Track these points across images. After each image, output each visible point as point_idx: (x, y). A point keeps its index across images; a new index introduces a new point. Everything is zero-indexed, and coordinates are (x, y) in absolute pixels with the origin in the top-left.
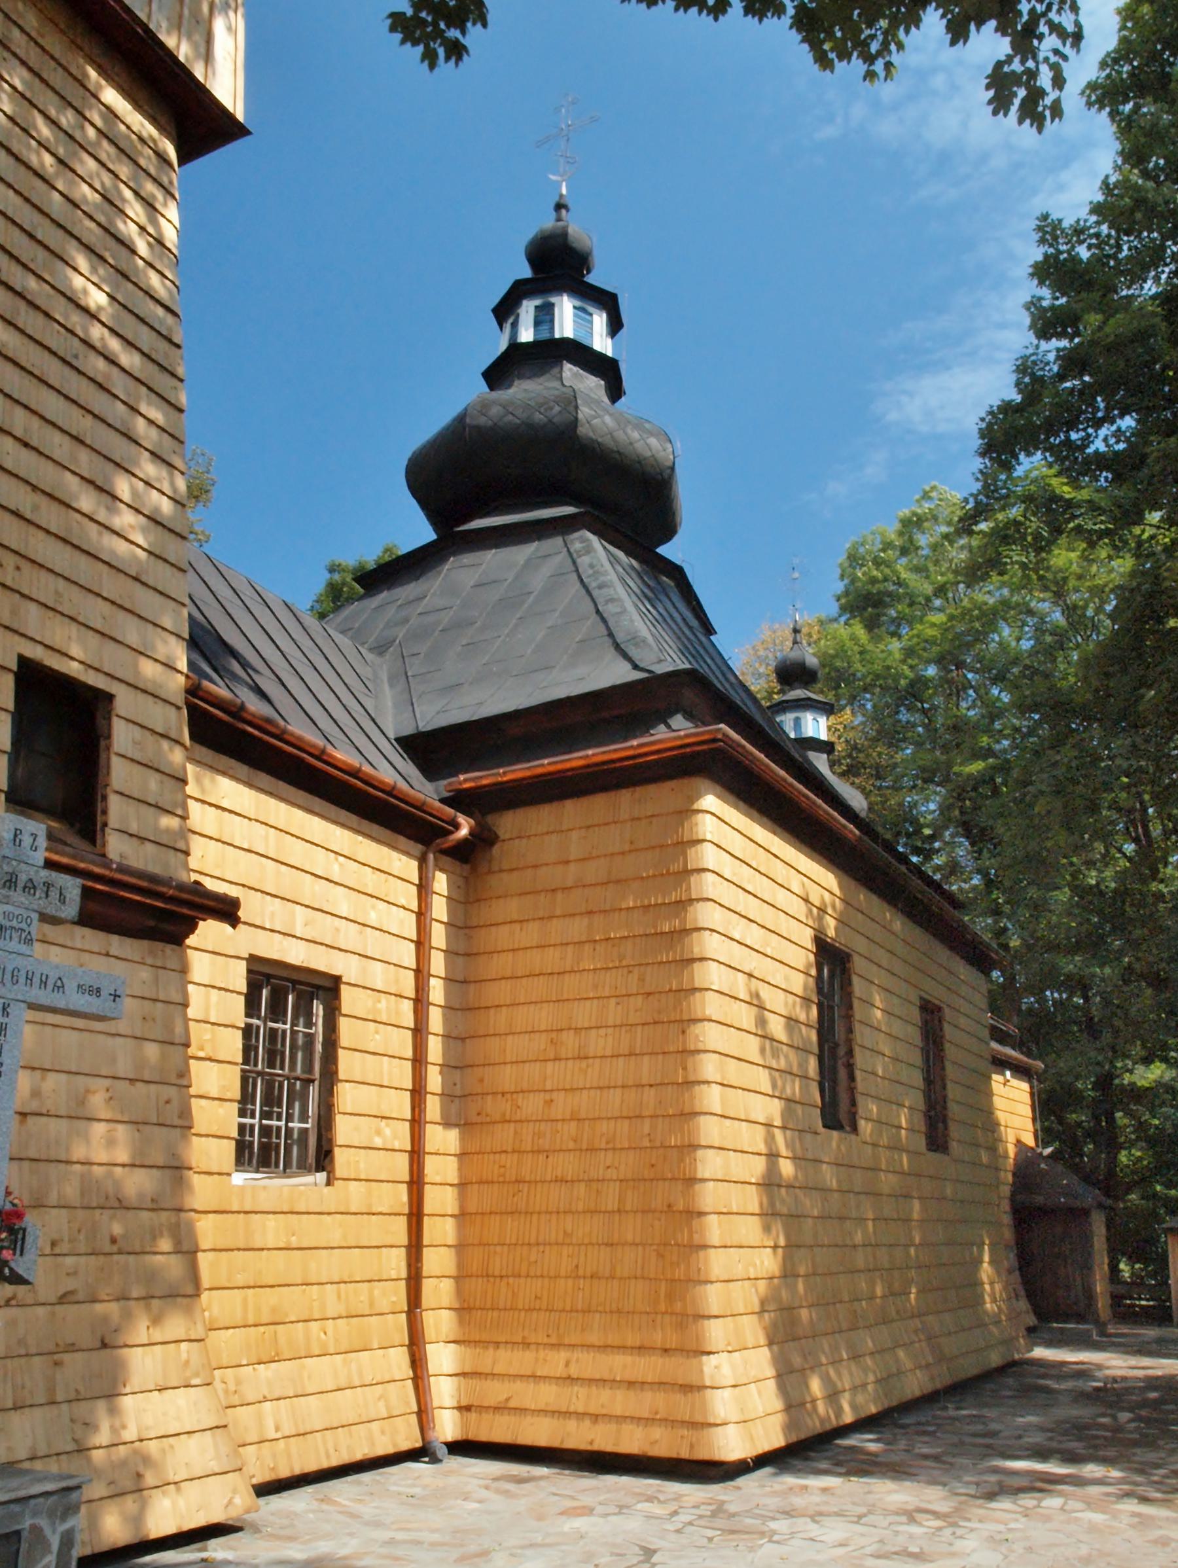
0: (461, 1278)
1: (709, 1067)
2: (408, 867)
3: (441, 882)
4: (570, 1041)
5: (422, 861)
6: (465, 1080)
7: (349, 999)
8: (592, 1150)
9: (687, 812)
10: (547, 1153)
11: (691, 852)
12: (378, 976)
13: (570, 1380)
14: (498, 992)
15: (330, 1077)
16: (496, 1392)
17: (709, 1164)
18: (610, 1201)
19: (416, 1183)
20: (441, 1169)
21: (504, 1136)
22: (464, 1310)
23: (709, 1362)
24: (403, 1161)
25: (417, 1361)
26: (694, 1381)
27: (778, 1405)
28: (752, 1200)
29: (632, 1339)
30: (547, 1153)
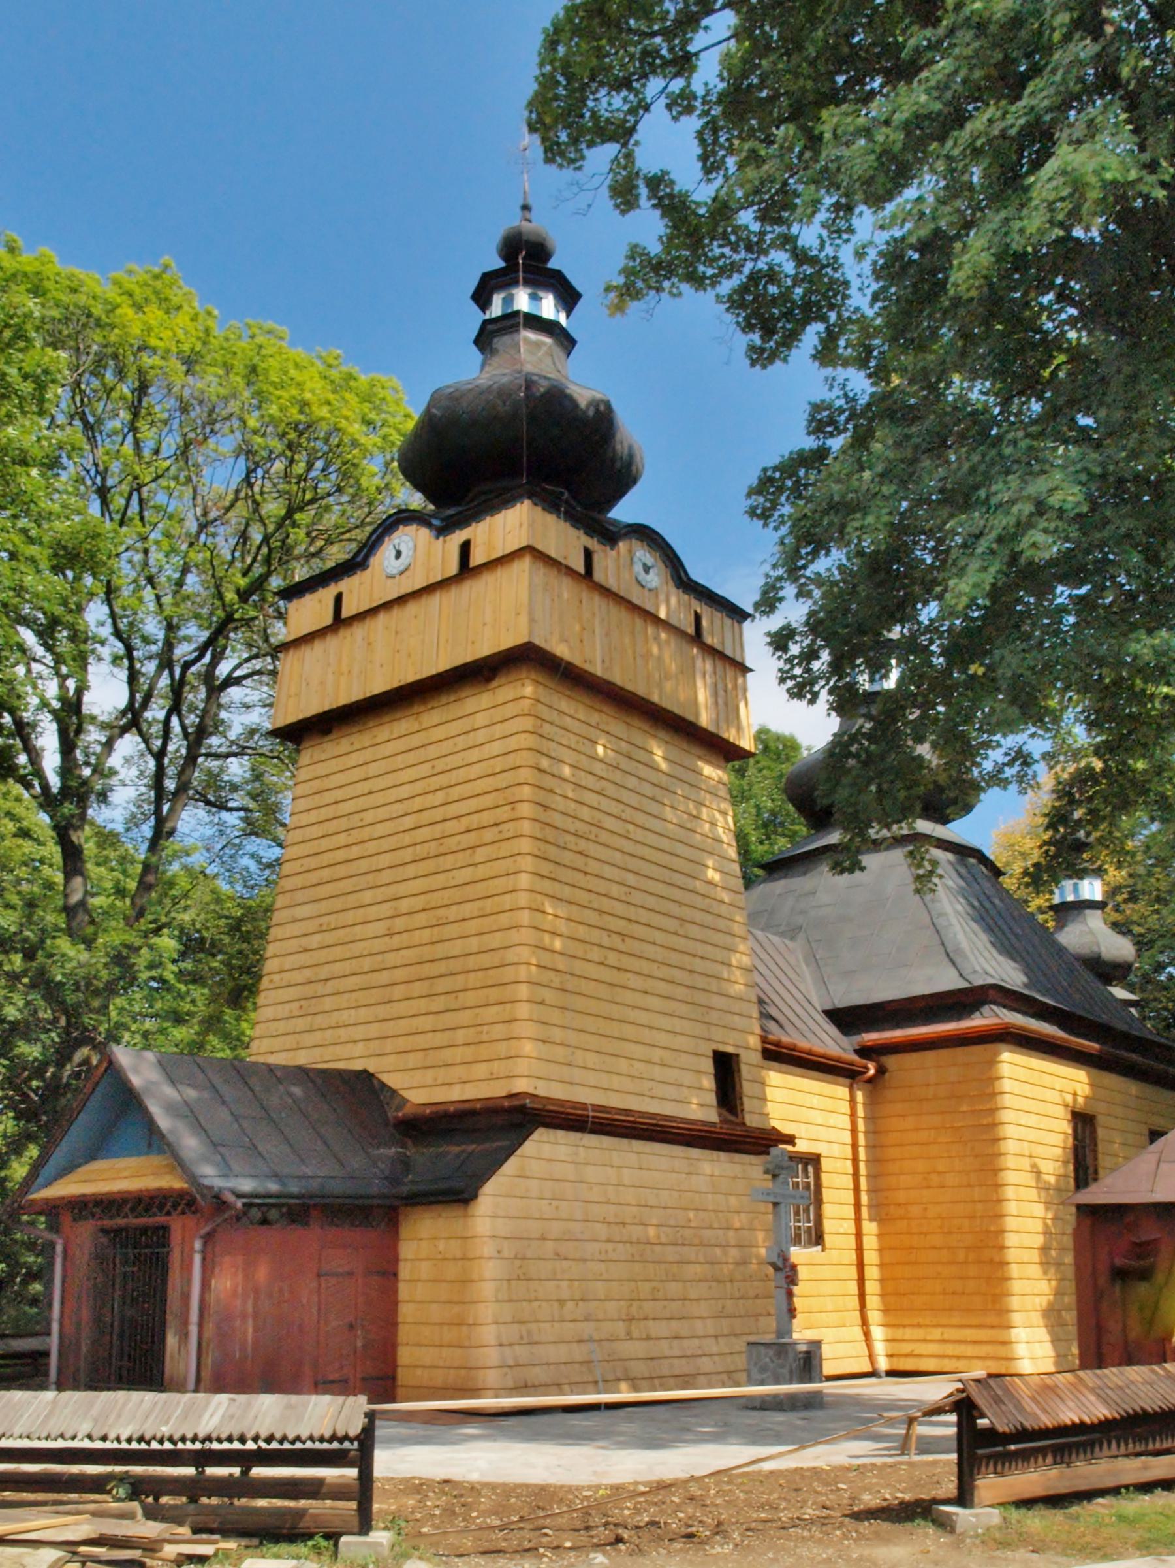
0: (883, 1295)
1: (1010, 1192)
2: (842, 1092)
3: (860, 1096)
4: (935, 1179)
5: (851, 1088)
6: (880, 1197)
7: (825, 1164)
8: (950, 1233)
9: (993, 1062)
10: (926, 1234)
11: (997, 1083)
12: (836, 1150)
13: (944, 1341)
14: (893, 1152)
15: (819, 1202)
16: (906, 1348)
17: (1011, 1240)
18: (961, 1256)
19: (860, 1249)
20: (870, 1242)
21: (902, 1225)
22: (886, 1311)
23: (1013, 1331)
24: (853, 1239)
25: (867, 1335)
26: (1006, 1339)
27: (1052, 1353)
28: (1035, 1256)
29: (975, 1321)
30: (926, 1234)
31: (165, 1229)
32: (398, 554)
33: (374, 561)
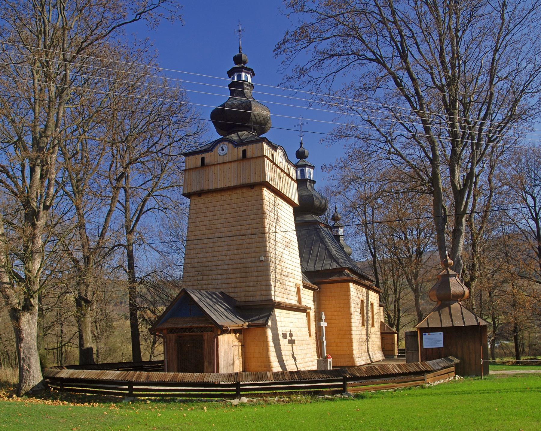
31: (202, 336)
32: (223, 150)
33: (215, 150)
